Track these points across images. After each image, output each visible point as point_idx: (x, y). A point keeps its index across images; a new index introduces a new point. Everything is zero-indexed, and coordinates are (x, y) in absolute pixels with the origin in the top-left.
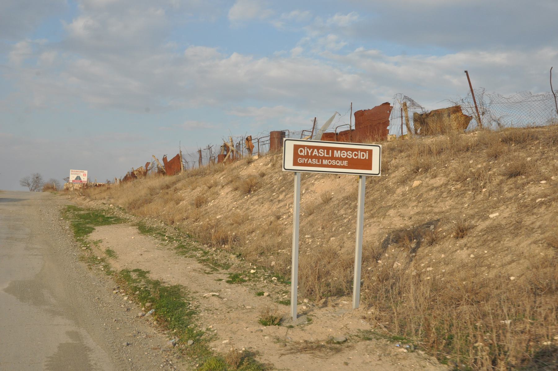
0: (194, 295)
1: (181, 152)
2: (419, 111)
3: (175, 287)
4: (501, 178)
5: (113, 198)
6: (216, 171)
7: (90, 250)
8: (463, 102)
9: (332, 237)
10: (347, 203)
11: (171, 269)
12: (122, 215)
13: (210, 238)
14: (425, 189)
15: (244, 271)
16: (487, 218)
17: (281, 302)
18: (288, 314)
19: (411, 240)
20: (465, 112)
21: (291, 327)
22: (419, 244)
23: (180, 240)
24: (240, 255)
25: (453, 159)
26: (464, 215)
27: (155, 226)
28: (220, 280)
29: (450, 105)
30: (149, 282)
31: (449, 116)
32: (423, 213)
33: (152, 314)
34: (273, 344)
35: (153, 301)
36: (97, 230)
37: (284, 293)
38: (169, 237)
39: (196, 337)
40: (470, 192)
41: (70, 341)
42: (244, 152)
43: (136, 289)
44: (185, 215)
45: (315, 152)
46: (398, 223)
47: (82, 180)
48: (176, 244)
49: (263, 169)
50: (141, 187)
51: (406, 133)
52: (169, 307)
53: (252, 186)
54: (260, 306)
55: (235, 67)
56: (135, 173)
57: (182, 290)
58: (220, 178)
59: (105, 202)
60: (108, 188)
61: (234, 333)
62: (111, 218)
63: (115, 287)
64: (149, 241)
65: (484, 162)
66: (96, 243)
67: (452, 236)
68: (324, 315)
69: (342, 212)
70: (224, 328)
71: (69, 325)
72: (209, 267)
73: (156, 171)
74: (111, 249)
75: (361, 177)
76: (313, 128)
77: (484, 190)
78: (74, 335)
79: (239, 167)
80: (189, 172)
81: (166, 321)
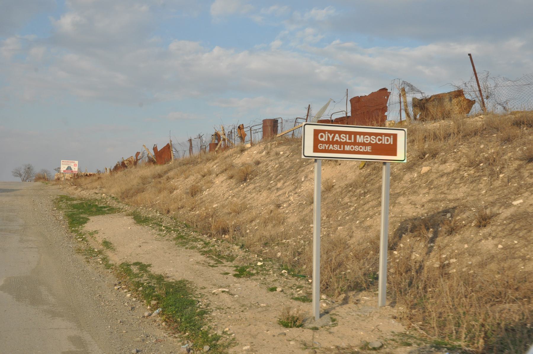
0: (203, 291)
1: (171, 141)
2: (419, 96)
3: (181, 282)
4: (518, 162)
5: (104, 187)
6: (208, 160)
7: (87, 241)
8: (466, 86)
9: (339, 226)
10: (350, 191)
11: (176, 263)
12: (115, 204)
13: (209, 228)
14: (435, 176)
15: (250, 264)
16: (511, 205)
17: (297, 299)
18: (308, 313)
19: (428, 229)
20: (467, 96)
21: (315, 329)
22: (436, 234)
23: (178, 230)
24: (243, 245)
25: (462, 144)
26: (483, 202)
27: (150, 216)
28: (227, 274)
29: (452, 89)
30: (151, 277)
31: (451, 100)
32: (437, 201)
33: (159, 314)
34: (300, 350)
35: (158, 298)
36: (91, 220)
37: (298, 288)
38: (166, 228)
39: (211, 341)
40: (486, 178)
41: (73, 348)
42: (237, 141)
43: (138, 284)
44: (180, 204)
45: (337, 137)
46: (410, 212)
47: (73, 170)
48: (175, 235)
49: (258, 157)
50: (132, 176)
51: (405, 119)
52: (177, 305)
53: (247, 174)
54: (275, 303)
55: (217, 60)
56: (126, 162)
57: (187, 285)
58: (213, 166)
59: (97, 192)
60: (99, 178)
61: (254, 337)
62: (105, 208)
63: (117, 282)
64: (146, 232)
65: (497, 146)
66: (91, 234)
67: (473, 224)
68: (348, 314)
69: (346, 200)
70: (241, 331)
71: (71, 328)
72: (213, 259)
73: (147, 160)
74: (107, 240)
75: (384, 163)
76: (308, 115)
77: (501, 176)
78: (77, 341)
79: (231, 155)
80: (180, 161)
81: (176, 322)
